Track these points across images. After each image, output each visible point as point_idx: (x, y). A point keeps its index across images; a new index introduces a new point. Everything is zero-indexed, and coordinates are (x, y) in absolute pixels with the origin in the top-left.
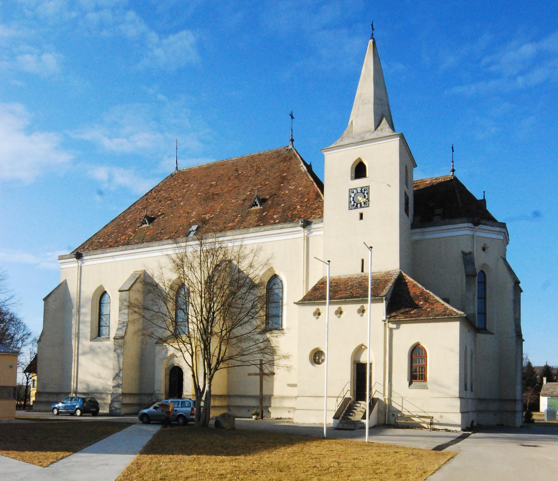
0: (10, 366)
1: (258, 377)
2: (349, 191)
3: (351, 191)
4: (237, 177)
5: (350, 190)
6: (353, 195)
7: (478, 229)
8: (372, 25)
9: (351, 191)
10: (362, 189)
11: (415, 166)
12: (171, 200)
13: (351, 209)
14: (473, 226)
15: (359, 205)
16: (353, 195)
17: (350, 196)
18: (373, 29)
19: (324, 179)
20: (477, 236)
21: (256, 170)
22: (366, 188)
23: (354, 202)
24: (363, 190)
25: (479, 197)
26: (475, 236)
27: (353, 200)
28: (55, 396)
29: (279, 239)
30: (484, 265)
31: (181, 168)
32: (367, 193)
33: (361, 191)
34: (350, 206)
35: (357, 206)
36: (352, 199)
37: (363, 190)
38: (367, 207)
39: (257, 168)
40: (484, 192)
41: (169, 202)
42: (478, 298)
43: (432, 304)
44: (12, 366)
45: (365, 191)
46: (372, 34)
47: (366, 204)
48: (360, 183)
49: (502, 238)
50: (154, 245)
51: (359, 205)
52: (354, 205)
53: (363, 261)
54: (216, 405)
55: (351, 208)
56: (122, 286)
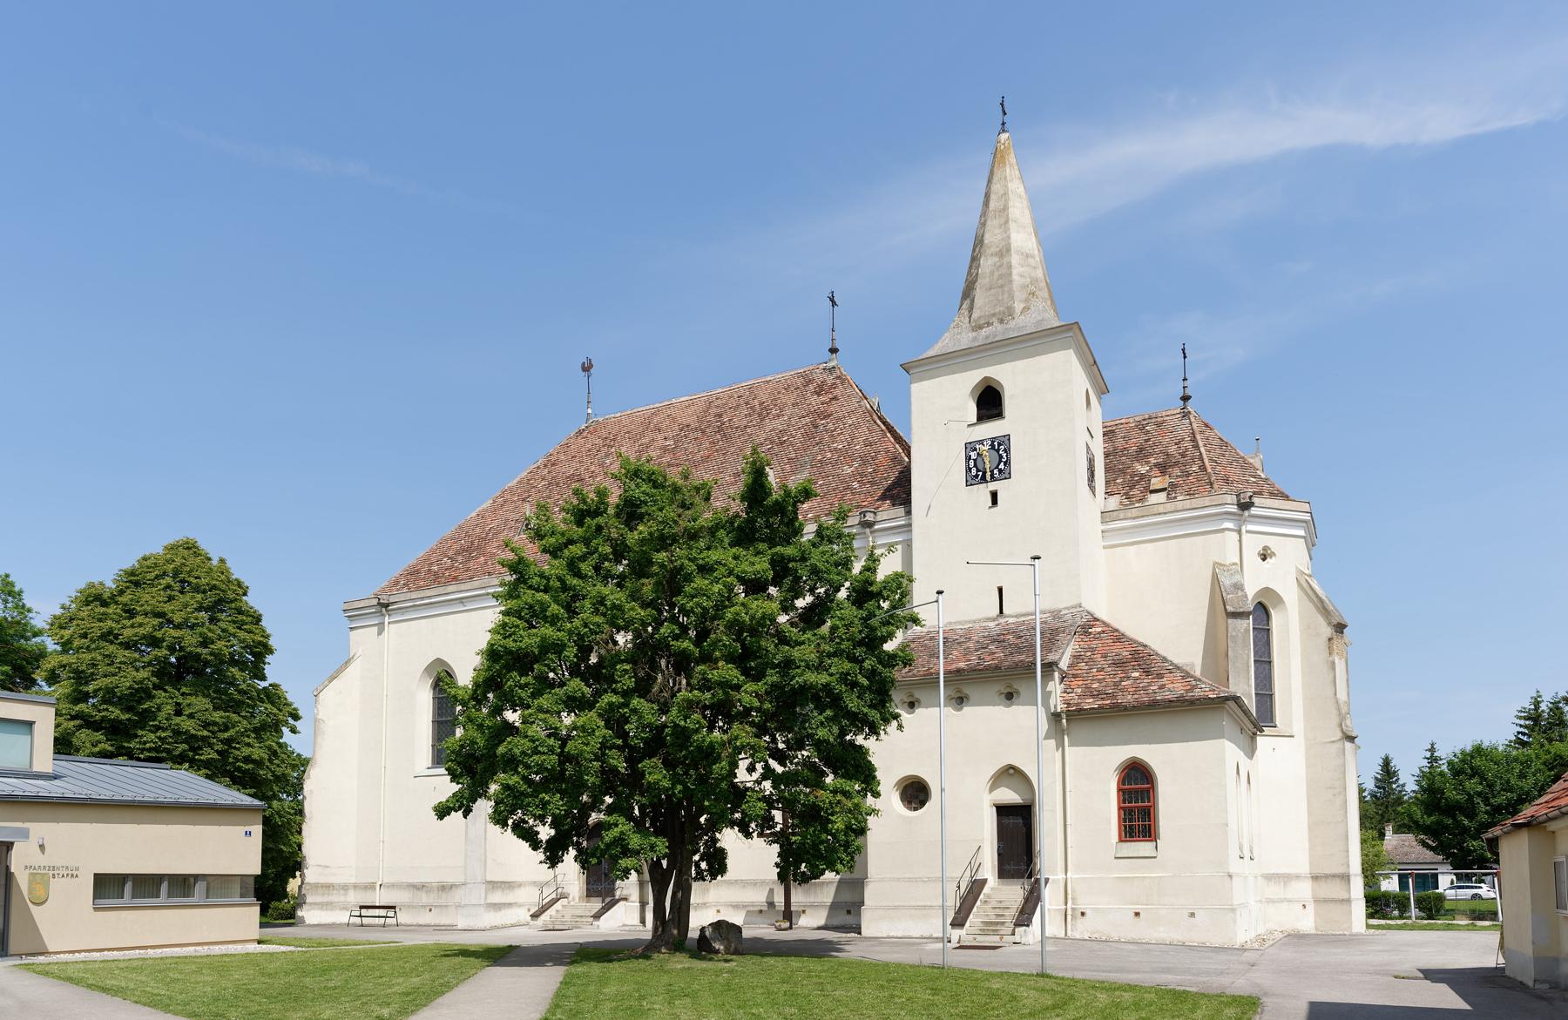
3: (970, 447)
4: (720, 430)
5: (968, 445)
6: (973, 455)
9: (970, 447)
10: (993, 442)
14: (1240, 512)
16: (973, 455)
17: (968, 458)
19: (910, 429)
20: (1247, 532)
22: (1002, 439)
23: (978, 470)
24: (996, 443)
27: (975, 466)
28: (342, 892)
29: (230, 946)
30: (1267, 591)
32: (1005, 451)
33: (992, 446)
34: (969, 479)
36: (972, 464)
37: (996, 443)
38: (1005, 478)
43: (1160, 676)
45: (1001, 446)
46: (1003, 124)
47: (1005, 474)
48: (992, 429)
52: (977, 476)
53: (1000, 590)
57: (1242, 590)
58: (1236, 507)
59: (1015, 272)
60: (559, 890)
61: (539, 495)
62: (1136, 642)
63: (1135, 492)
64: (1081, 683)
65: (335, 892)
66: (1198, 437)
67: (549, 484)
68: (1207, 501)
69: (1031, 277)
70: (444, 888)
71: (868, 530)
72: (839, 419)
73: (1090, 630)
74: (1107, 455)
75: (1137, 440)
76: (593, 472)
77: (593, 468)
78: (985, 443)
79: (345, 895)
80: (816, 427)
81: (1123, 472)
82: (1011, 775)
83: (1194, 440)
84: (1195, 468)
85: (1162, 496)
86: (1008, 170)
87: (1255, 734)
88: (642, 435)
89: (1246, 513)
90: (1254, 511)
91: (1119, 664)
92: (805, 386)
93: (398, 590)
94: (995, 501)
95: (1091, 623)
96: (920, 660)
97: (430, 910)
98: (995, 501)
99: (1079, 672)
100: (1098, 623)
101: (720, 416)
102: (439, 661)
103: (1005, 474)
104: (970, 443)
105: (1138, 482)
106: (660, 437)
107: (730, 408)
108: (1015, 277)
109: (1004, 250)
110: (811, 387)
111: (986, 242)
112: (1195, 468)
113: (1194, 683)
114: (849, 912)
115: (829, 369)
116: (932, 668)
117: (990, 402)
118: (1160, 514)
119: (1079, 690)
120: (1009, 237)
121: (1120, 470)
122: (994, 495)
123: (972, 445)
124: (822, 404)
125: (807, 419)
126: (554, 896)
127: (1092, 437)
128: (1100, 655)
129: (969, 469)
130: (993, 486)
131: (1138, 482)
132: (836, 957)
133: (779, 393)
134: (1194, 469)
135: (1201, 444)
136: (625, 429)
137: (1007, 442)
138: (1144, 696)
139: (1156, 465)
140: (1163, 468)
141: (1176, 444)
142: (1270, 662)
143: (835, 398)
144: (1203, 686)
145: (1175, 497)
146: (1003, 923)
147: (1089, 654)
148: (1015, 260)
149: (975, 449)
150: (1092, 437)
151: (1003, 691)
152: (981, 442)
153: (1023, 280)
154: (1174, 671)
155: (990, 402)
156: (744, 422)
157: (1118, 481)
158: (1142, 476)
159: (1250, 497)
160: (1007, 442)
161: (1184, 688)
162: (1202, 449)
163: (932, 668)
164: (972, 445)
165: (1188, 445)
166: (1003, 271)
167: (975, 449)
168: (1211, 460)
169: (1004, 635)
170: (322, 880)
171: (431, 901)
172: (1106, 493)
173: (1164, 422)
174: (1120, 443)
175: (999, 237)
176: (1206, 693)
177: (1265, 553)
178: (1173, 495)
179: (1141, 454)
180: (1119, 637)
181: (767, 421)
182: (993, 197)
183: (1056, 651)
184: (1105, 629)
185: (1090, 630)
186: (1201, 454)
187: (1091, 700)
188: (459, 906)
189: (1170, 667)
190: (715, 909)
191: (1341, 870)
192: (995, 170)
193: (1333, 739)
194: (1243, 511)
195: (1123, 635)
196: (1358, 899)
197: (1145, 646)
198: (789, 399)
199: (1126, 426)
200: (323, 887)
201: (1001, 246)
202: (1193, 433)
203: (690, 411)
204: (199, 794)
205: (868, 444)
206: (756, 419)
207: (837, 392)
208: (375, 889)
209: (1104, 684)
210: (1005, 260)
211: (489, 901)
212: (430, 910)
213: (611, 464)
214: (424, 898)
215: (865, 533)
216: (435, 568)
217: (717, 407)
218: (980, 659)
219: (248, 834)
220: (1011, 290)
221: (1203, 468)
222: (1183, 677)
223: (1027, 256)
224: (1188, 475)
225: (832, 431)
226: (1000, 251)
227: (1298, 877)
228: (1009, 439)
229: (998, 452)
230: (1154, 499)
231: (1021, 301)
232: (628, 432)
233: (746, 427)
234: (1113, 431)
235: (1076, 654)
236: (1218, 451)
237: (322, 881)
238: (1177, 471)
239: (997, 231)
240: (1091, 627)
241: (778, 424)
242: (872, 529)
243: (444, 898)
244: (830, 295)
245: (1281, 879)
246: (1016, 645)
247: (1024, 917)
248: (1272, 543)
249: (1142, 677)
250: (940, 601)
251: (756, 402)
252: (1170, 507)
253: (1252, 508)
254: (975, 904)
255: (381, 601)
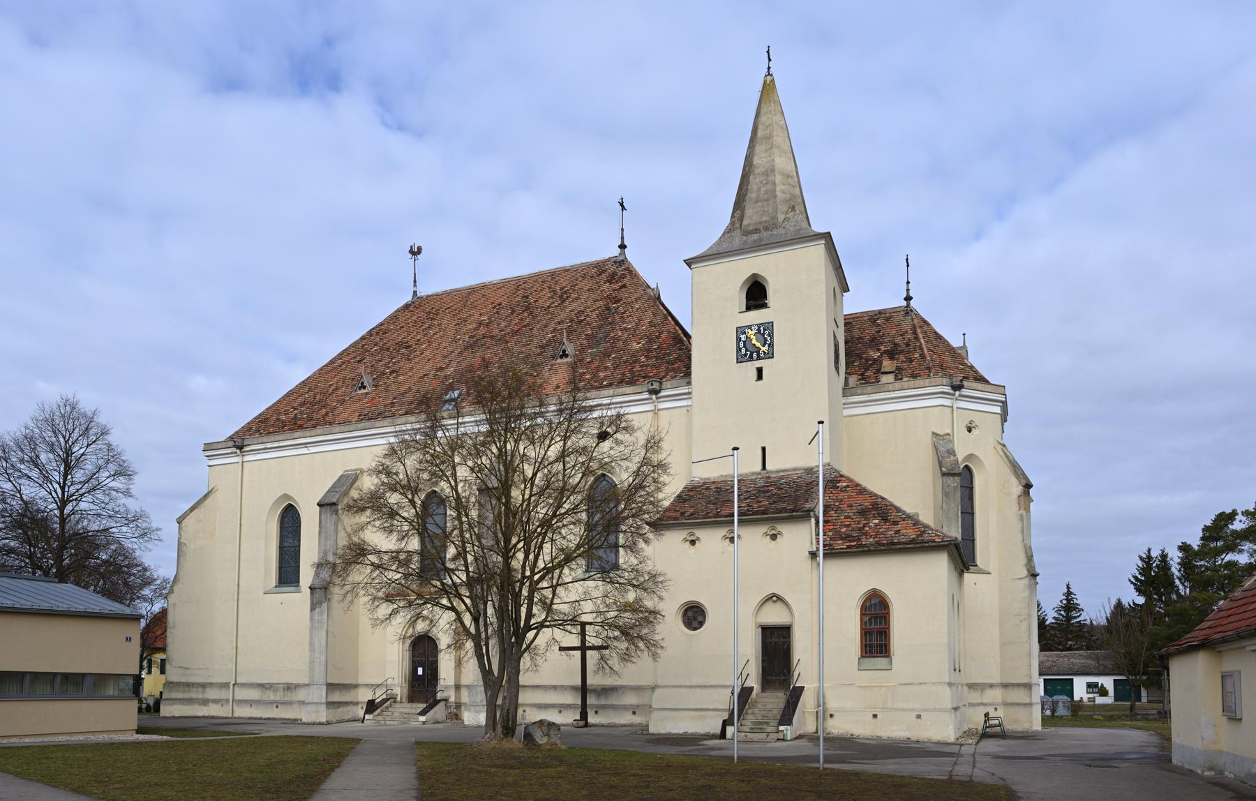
0: (127, 638)
1: (578, 654)
2: (737, 331)
3: (741, 330)
6: (743, 337)
7: (960, 396)
8: (768, 52)
9: (741, 330)
10: (759, 328)
11: (846, 290)
12: (406, 347)
13: (741, 362)
14: (952, 392)
15: (755, 355)
17: (739, 340)
18: (770, 60)
20: (958, 408)
21: (561, 297)
23: (747, 350)
24: (762, 328)
25: (956, 342)
26: (955, 408)
27: (744, 346)
28: (200, 689)
31: (424, 291)
32: (769, 335)
33: (759, 330)
34: (739, 357)
35: (751, 356)
36: (742, 344)
37: (762, 328)
39: (562, 293)
40: (964, 335)
41: (404, 351)
42: (962, 513)
43: (896, 523)
44: (130, 638)
45: (766, 331)
46: (769, 68)
48: (757, 316)
49: (998, 410)
50: (377, 425)
51: (755, 355)
52: (746, 355)
53: (764, 449)
54: (176, 716)
55: (740, 359)
56: (324, 496)
57: (955, 456)
58: (950, 388)
59: (778, 189)
60: (389, 692)
61: (372, 358)
62: (876, 495)
63: (869, 373)
64: (831, 527)
65: (194, 690)
66: (919, 330)
67: (381, 349)
68: (927, 382)
69: (790, 194)
70: (289, 687)
71: (654, 397)
72: (628, 303)
73: (838, 485)
74: (846, 342)
75: (869, 331)
76: (419, 340)
77: (418, 338)
78: (753, 328)
79: (203, 692)
80: (609, 309)
81: (859, 356)
82: (775, 602)
83: (915, 332)
84: (916, 355)
85: (891, 378)
86: (772, 105)
87: (963, 572)
88: (461, 311)
89: (957, 393)
90: (965, 392)
91: (863, 512)
92: (599, 276)
93: (251, 435)
94: (760, 376)
95: (839, 479)
96: (699, 505)
97: (277, 707)
98: (760, 376)
99: (830, 518)
100: (843, 479)
101: (527, 297)
102: (286, 496)
103: (770, 355)
104: (740, 327)
105: (871, 365)
106: (476, 313)
107: (536, 291)
108: (779, 194)
109: (769, 171)
110: (604, 276)
111: (755, 163)
112: (916, 355)
113: (923, 529)
114: (634, 713)
115: (619, 262)
116: (710, 513)
117: (756, 294)
118: (889, 391)
119: (831, 534)
120: (773, 160)
121: (857, 355)
122: (760, 371)
123: (742, 329)
124: (614, 290)
125: (601, 303)
126: (384, 696)
127: (838, 327)
128: (846, 505)
129: (739, 349)
130: (758, 364)
131: (871, 365)
132: (703, 745)
133: (577, 280)
134: (916, 356)
135: (921, 336)
136: (446, 306)
137: (770, 328)
138: (883, 539)
139: (885, 352)
140: (891, 355)
141: (901, 335)
142: (973, 514)
143: (624, 286)
144: (930, 532)
145: (901, 379)
146: (767, 723)
147: (837, 504)
148: (778, 179)
149: (745, 333)
150: (838, 327)
151: (768, 533)
152: (750, 327)
153: (784, 196)
154: (906, 519)
155: (756, 294)
156: (548, 303)
157: (855, 364)
158: (875, 361)
159: (961, 381)
160: (770, 328)
161: (916, 533)
162: (922, 341)
163: (710, 513)
164: (742, 329)
165: (910, 336)
166: (769, 187)
167: (745, 333)
168: (929, 350)
169: (767, 486)
170: (184, 680)
171: (278, 699)
172: (846, 373)
173: (891, 317)
174: (856, 333)
175: (765, 160)
176: (933, 538)
177: (970, 425)
178: (900, 377)
179: (874, 342)
180: (861, 491)
181: (567, 303)
182: (760, 127)
183: (812, 501)
184: (849, 484)
185: (838, 485)
186: (921, 344)
187: (841, 542)
188: (302, 703)
189: (904, 516)
190: (595, 710)
191: (1025, 680)
192: (762, 105)
193: (1021, 577)
194: (955, 391)
195: (864, 489)
196: (1037, 703)
197: (883, 498)
198: (586, 284)
199: (860, 319)
200: (184, 685)
201: (766, 167)
202: (914, 327)
203: (501, 292)
204: (71, 603)
205: (652, 325)
206: (557, 301)
207: (626, 281)
208: (229, 687)
209: (850, 529)
210: (771, 178)
211: (329, 700)
212: (277, 707)
213: (434, 334)
214: (271, 696)
215: (651, 399)
216: (283, 417)
217: (524, 289)
218: (748, 506)
219: (129, 639)
220: (775, 203)
221: (923, 356)
222: (914, 525)
223: (788, 176)
224: (911, 361)
225: (623, 313)
226: (766, 171)
227: (991, 686)
228: (773, 326)
229: (764, 336)
230: (885, 379)
231: (783, 213)
232: (449, 308)
233: (549, 307)
234: (851, 323)
235: (827, 504)
236: (934, 342)
237: (184, 681)
238: (902, 358)
239: (763, 155)
240: (839, 482)
241: (577, 306)
242: (658, 395)
243: (289, 697)
244: (621, 201)
245: (979, 687)
246: (779, 495)
247: (787, 717)
248: (977, 418)
249: (881, 524)
250: (735, 455)
251: (558, 287)
252: (897, 385)
253: (963, 390)
254: (744, 707)
255: (237, 444)
